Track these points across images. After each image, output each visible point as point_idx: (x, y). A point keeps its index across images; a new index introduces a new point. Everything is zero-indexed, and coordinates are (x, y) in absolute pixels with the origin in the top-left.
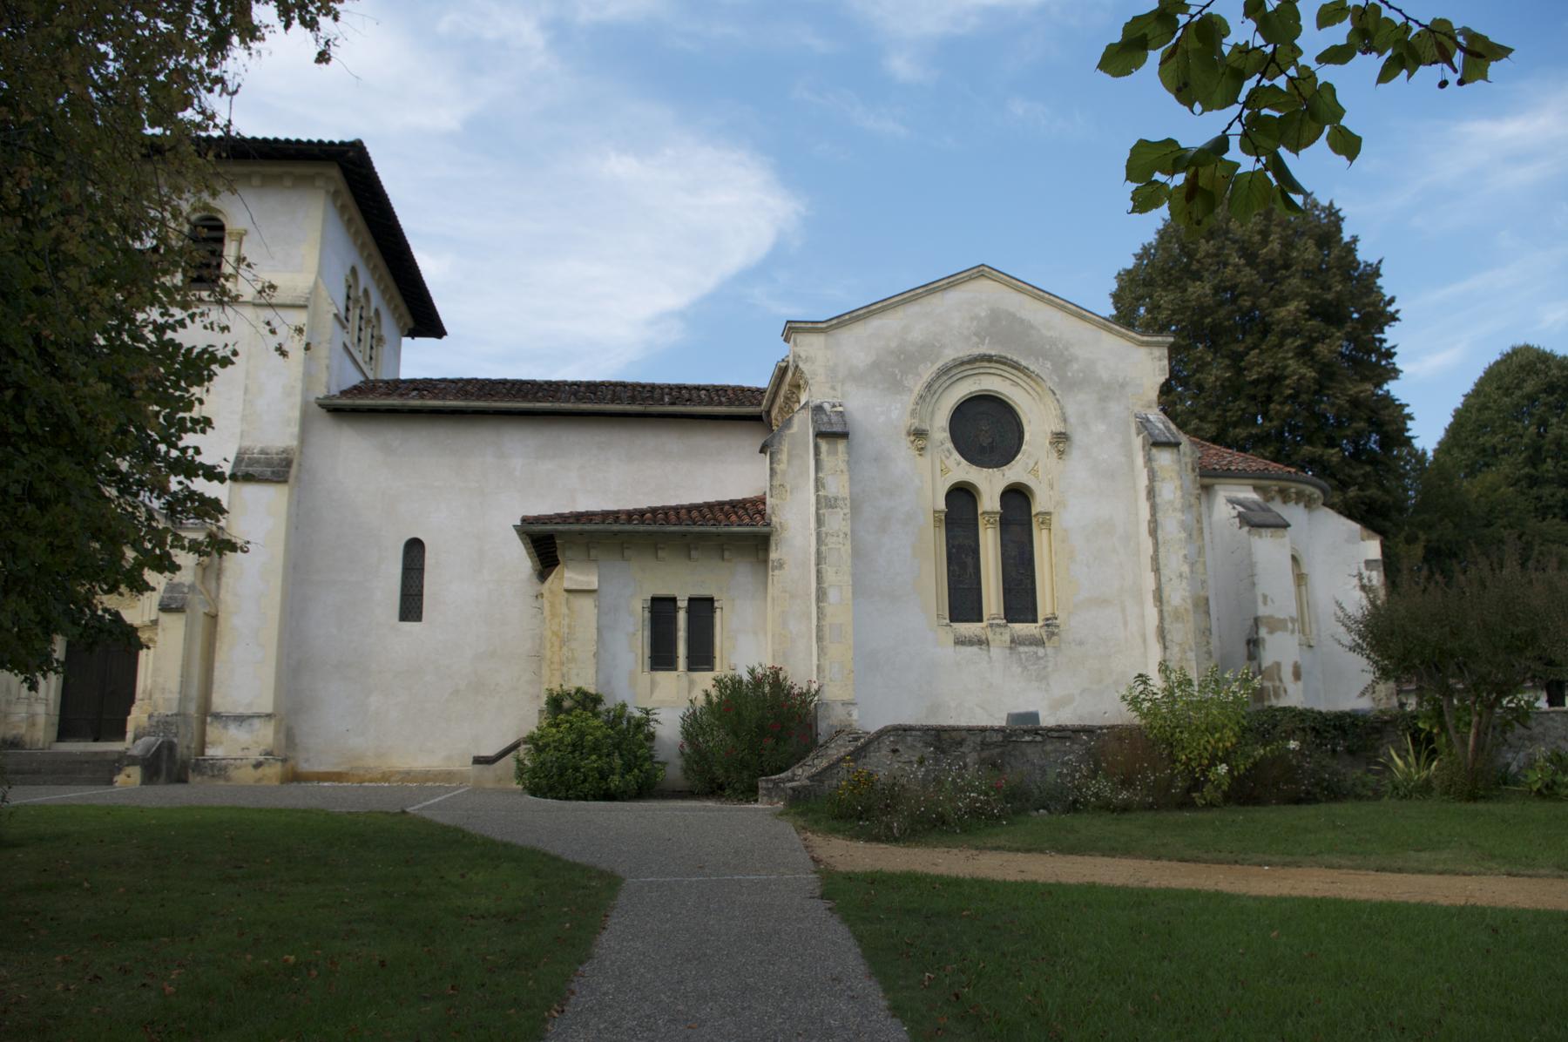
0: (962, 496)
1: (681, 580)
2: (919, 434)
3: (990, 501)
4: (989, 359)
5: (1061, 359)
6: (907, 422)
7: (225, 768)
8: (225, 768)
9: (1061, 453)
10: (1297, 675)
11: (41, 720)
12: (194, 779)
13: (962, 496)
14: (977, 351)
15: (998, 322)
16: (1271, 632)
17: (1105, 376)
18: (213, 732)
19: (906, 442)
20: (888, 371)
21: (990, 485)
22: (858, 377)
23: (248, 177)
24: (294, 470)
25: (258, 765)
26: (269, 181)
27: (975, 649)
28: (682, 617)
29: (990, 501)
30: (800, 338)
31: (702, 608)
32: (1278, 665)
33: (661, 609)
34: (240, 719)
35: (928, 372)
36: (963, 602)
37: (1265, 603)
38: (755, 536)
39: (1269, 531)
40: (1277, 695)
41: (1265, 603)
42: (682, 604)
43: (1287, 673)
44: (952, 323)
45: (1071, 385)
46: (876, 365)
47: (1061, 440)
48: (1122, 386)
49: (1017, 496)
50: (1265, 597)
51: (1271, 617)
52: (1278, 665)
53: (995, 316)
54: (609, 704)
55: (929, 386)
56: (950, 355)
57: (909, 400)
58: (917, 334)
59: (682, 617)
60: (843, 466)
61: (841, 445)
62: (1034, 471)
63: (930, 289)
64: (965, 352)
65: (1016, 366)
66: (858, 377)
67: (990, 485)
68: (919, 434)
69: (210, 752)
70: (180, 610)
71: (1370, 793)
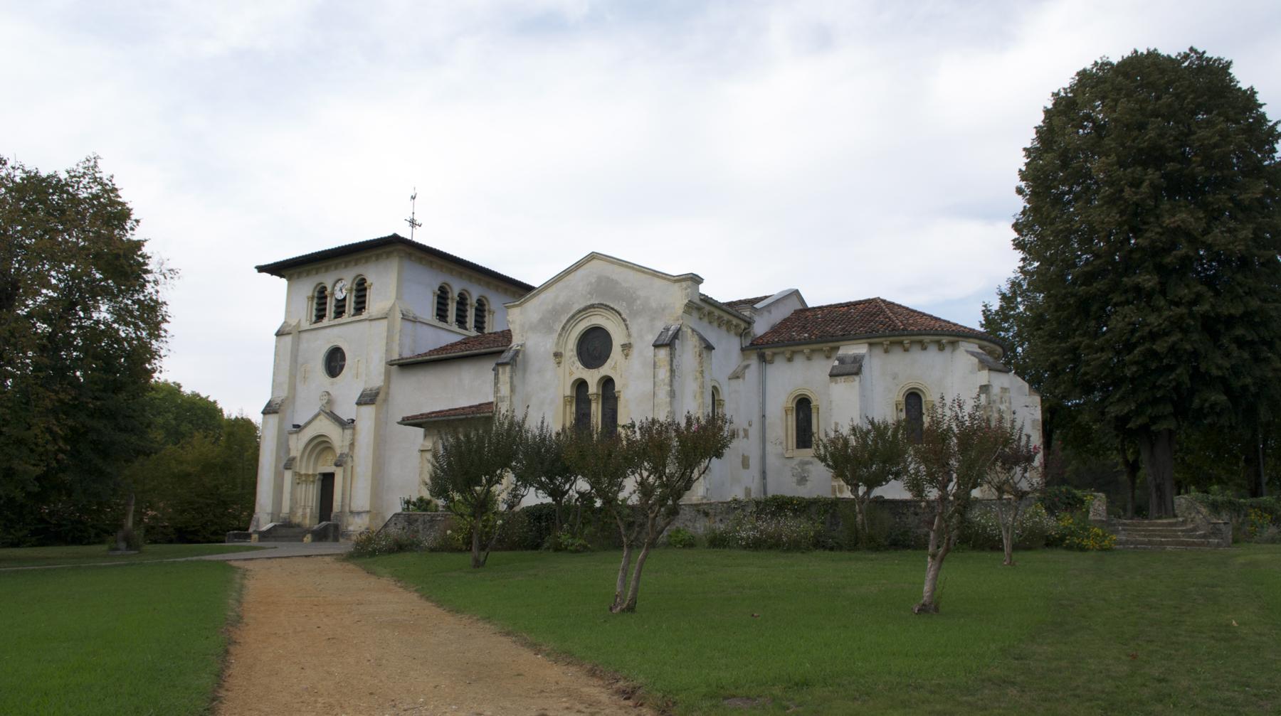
0: (581, 385)
2: (557, 355)
3: (593, 389)
4: (592, 306)
6: (554, 350)
13: (581, 385)
17: (654, 305)
19: (552, 360)
20: (544, 325)
21: (593, 378)
22: (533, 328)
30: (345, 418)
34: (359, 513)
46: (541, 320)
48: (663, 310)
49: (607, 383)
55: (563, 328)
56: (577, 307)
57: (556, 335)
58: (561, 300)
62: (614, 368)
63: (567, 272)
64: (582, 306)
65: (607, 307)
66: (533, 328)
67: (593, 378)
68: (557, 355)
70: (275, 412)
71: (1131, 458)
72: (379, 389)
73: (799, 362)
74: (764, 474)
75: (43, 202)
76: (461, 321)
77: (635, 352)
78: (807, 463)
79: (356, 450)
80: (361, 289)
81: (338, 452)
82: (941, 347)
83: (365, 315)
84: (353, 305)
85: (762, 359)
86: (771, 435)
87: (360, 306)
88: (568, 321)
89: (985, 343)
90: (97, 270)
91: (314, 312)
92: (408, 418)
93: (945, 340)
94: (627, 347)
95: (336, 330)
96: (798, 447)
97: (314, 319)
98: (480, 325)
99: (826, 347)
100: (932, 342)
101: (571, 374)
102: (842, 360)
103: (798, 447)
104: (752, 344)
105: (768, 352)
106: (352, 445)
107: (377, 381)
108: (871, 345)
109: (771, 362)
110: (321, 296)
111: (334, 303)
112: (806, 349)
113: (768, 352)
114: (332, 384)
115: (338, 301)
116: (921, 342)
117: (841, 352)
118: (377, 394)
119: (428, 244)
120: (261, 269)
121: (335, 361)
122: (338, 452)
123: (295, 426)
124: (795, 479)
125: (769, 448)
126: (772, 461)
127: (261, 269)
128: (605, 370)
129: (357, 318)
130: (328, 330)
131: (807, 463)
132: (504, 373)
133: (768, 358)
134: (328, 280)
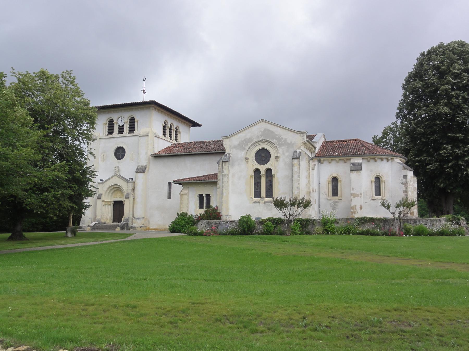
1: (204, 191)
2: (247, 159)
3: (263, 172)
4: (262, 140)
5: (279, 139)
7: (135, 228)
8: (135, 228)
9: (277, 160)
10: (361, 208)
11: (109, 219)
12: (131, 230)
13: (257, 171)
14: (260, 139)
15: (266, 131)
16: (354, 197)
18: (134, 221)
19: (244, 160)
20: (241, 146)
21: (263, 168)
22: (235, 147)
23: (138, 108)
24: (146, 170)
25: (141, 227)
26: (141, 109)
27: (257, 204)
28: (205, 198)
29: (263, 172)
31: (208, 196)
32: (356, 206)
33: (201, 196)
34: (138, 218)
35: (250, 144)
36: (257, 194)
37: (353, 190)
38: (215, 182)
39: (356, 171)
40: (355, 213)
41: (353, 190)
42: (204, 196)
43: (358, 208)
44: (255, 132)
45: (280, 145)
46: (239, 144)
47: (277, 157)
49: (269, 171)
50: (353, 188)
51: (354, 193)
52: (356, 206)
53: (265, 130)
54: (189, 214)
55: (249, 148)
56: (255, 140)
57: (245, 151)
58: (248, 137)
59: (205, 198)
60: (227, 168)
61: (227, 163)
64: (257, 140)
66: (235, 147)
67: (263, 168)
69: (134, 225)
70: (128, 198)
72: (146, 166)
73: (334, 163)
74: (319, 206)
75: (427, 135)
76: (170, 137)
77: (281, 159)
78: (337, 202)
79: (136, 192)
80: (132, 122)
81: (125, 192)
82: (388, 160)
83: (136, 133)
84: (128, 129)
85: (319, 162)
86: (322, 191)
87: (132, 130)
88: (251, 146)
89: (402, 159)
90: (452, 164)
91: (107, 130)
92: (176, 181)
93: (390, 158)
94: (277, 157)
95: (120, 139)
96: (332, 196)
97: (107, 133)
98: (176, 140)
99: (345, 158)
100: (379, 158)
101: (253, 166)
102: (353, 164)
103: (332, 196)
104: (316, 156)
105: (322, 159)
106: (133, 189)
107: (143, 163)
108: (363, 158)
109: (322, 163)
110: (111, 124)
111: (118, 127)
112: (337, 159)
113: (322, 159)
114: (119, 163)
115: (119, 126)
116: (374, 159)
117: (352, 161)
118: (145, 168)
119: (161, 103)
120: (200, 125)
121: (120, 153)
122: (125, 192)
123: (101, 180)
124: (332, 208)
125: (321, 196)
126: (322, 200)
127: (200, 125)
128: (268, 166)
129: (130, 135)
130: (116, 139)
131: (337, 202)
132: (225, 165)
133: (322, 162)
134: (115, 116)
